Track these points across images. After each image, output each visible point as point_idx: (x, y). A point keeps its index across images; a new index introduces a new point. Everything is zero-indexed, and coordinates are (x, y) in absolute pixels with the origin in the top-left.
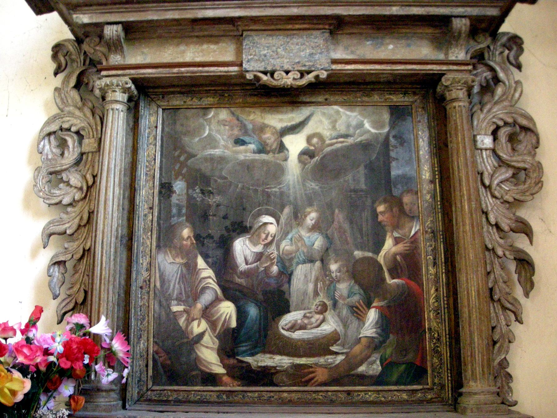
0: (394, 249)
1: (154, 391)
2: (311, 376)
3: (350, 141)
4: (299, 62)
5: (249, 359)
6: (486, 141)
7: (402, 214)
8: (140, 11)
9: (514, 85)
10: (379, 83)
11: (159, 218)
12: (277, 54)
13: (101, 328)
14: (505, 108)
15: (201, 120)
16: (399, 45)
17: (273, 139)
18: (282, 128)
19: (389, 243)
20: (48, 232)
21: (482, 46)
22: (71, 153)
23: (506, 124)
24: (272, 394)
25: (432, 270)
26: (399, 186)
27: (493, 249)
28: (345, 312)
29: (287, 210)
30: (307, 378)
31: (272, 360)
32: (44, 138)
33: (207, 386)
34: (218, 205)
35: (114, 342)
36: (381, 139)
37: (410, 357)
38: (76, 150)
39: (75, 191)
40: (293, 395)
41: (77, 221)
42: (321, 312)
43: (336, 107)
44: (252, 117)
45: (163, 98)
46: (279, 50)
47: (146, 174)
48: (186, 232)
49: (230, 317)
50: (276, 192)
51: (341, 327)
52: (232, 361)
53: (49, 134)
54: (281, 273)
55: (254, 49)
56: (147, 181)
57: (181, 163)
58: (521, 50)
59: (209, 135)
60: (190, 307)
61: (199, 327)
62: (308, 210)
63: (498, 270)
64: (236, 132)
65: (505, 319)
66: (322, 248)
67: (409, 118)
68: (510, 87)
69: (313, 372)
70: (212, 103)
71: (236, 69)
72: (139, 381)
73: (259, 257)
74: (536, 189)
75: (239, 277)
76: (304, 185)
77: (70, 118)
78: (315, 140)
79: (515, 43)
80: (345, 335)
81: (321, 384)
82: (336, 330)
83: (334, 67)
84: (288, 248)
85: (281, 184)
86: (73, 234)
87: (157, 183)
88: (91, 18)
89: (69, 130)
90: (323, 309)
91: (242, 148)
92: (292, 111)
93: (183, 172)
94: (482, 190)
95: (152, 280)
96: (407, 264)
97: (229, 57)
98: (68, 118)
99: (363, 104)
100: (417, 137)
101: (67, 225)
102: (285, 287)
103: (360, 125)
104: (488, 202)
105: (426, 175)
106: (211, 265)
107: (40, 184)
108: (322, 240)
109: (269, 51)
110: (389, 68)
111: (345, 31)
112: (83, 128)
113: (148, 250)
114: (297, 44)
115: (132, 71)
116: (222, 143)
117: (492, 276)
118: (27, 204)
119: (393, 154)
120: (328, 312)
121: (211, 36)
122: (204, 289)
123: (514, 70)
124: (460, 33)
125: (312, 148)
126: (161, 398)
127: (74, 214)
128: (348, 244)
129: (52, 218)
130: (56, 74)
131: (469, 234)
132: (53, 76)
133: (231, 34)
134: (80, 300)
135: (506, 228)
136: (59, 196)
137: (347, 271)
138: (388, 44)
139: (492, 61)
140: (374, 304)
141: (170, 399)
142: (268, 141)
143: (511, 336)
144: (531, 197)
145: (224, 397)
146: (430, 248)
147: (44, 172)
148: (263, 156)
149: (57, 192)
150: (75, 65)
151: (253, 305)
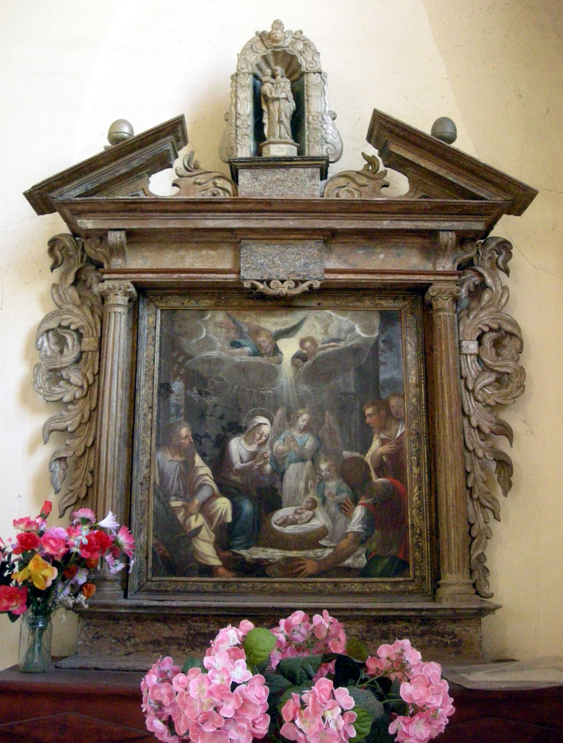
0: (381, 450)
1: (154, 581)
2: (301, 568)
3: (342, 345)
4: (294, 272)
5: (243, 552)
6: (472, 347)
7: (388, 416)
8: (143, 219)
9: (501, 291)
10: (370, 289)
11: (158, 417)
12: (273, 263)
13: (109, 522)
14: (491, 313)
15: (199, 322)
16: (389, 255)
17: (267, 343)
18: (276, 331)
19: (376, 443)
20: (50, 428)
21: (469, 255)
22: (71, 351)
23: (491, 330)
24: (265, 585)
25: (416, 470)
26: (387, 389)
27: (474, 451)
28: (333, 509)
29: (280, 412)
30: (297, 570)
31: (265, 553)
32: (42, 335)
33: (203, 577)
34: (215, 406)
35: (119, 535)
36: (371, 343)
37: (394, 551)
38: (75, 348)
39: (76, 389)
40: (285, 585)
41: (78, 419)
42: (311, 509)
43: (328, 311)
44: (247, 320)
45: (161, 298)
46: (275, 259)
47: (146, 374)
48: (184, 431)
49: (226, 512)
50: (270, 394)
51: (330, 523)
52: (227, 554)
53: (47, 331)
54: (274, 471)
55: (252, 258)
56: (146, 381)
57: (179, 364)
58: (509, 255)
59: (206, 337)
60: (188, 501)
61: (196, 521)
62: (301, 411)
63: (478, 471)
64: (232, 334)
65: (484, 517)
66: (312, 449)
67: (398, 323)
68: (497, 292)
69: (303, 565)
70: (209, 305)
71: (234, 276)
72: (139, 573)
73: (253, 456)
74: (518, 392)
75: (234, 475)
76: (297, 387)
77: (69, 316)
78: (308, 344)
79: (505, 248)
80: (334, 529)
81: (310, 576)
82: (324, 525)
83: (327, 276)
84: (281, 447)
85: (275, 386)
86: (74, 432)
87: (156, 383)
88: (95, 223)
89: (68, 327)
90: (313, 505)
91: (238, 350)
92: (287, 314)
93: (182, 373)
94: (465, 394)
95: (152, 477)
96: (393, 464)
97: (227, 265)
98: (67, 316)
99: (356, 309)
100: (405, 342)
101: (69, 423)
102: (277, 485)
103: (352, 329)
104: (471, 405)
105: (413, 379)
106: (209, 463)
107: (40, 381)
108: (313, 440)
109: (266, 260)
110: (379, 278)
111: (339, 240)
112: (83, 327)
113: (148, 448)
114: (292, 254)
115: (134, 276)
116: (219, 345)
117: (472, 476)
118: (24, 398)
119: (381, 359)
120: (317, 509)
121: (210, 242)
122: (202, 486)
123: (502, 274)
124: (446, 246)
125: (305, 352)
126: (160, 588)
127: (74, 412)
128: (337, 444)
129: (52, 415)
130: (52, 269)
131: (449, 438)
132: (49, 269)
133: (230, 240)
134: (83, 495)
135: (487, 431)
136: (59, 394)
137: (336, 470)
138: (379, 254)
139: (481, 266)
140: (361, 502)
141: (169, 589)
142: (263, 344)
143: (489, 532)
144: (512, 401)
145: (220, 587)
146: (415, 450)
147: (44, 369)
148: (258, 359)
149: (58, 390)
150: (72, 261)
151: (247, 501)
